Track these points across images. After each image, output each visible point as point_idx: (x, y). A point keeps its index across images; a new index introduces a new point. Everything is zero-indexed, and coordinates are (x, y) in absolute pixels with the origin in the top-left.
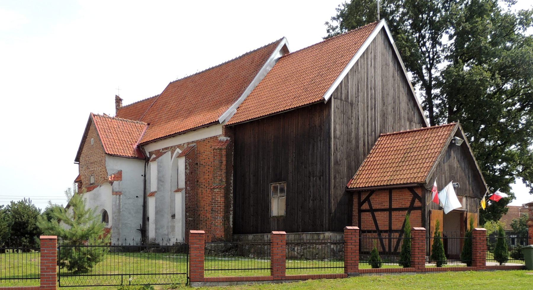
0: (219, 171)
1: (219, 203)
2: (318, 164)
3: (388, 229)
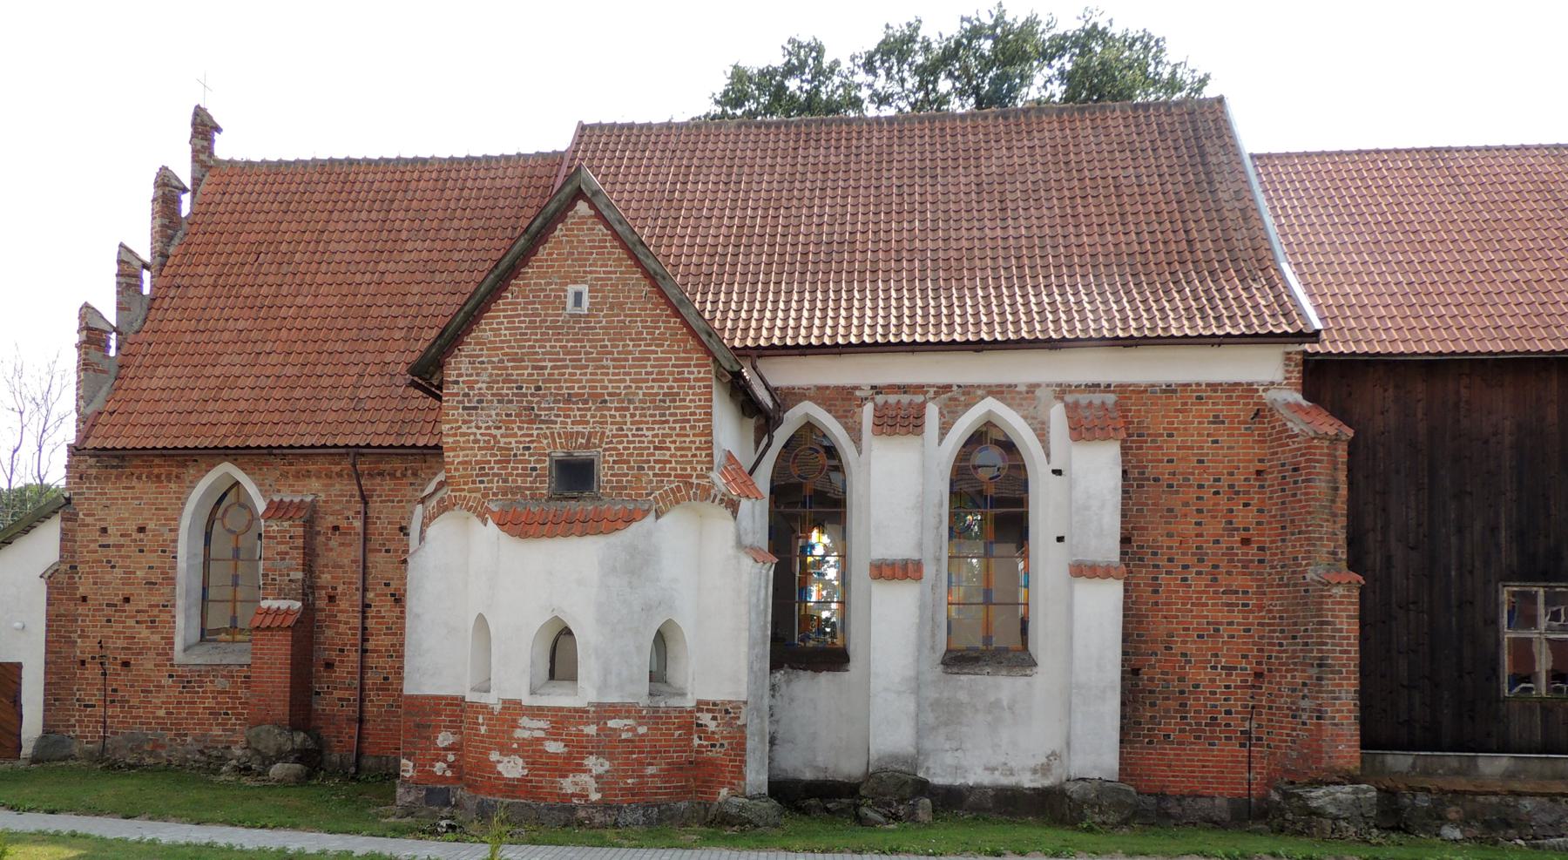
0: (1328, 521)
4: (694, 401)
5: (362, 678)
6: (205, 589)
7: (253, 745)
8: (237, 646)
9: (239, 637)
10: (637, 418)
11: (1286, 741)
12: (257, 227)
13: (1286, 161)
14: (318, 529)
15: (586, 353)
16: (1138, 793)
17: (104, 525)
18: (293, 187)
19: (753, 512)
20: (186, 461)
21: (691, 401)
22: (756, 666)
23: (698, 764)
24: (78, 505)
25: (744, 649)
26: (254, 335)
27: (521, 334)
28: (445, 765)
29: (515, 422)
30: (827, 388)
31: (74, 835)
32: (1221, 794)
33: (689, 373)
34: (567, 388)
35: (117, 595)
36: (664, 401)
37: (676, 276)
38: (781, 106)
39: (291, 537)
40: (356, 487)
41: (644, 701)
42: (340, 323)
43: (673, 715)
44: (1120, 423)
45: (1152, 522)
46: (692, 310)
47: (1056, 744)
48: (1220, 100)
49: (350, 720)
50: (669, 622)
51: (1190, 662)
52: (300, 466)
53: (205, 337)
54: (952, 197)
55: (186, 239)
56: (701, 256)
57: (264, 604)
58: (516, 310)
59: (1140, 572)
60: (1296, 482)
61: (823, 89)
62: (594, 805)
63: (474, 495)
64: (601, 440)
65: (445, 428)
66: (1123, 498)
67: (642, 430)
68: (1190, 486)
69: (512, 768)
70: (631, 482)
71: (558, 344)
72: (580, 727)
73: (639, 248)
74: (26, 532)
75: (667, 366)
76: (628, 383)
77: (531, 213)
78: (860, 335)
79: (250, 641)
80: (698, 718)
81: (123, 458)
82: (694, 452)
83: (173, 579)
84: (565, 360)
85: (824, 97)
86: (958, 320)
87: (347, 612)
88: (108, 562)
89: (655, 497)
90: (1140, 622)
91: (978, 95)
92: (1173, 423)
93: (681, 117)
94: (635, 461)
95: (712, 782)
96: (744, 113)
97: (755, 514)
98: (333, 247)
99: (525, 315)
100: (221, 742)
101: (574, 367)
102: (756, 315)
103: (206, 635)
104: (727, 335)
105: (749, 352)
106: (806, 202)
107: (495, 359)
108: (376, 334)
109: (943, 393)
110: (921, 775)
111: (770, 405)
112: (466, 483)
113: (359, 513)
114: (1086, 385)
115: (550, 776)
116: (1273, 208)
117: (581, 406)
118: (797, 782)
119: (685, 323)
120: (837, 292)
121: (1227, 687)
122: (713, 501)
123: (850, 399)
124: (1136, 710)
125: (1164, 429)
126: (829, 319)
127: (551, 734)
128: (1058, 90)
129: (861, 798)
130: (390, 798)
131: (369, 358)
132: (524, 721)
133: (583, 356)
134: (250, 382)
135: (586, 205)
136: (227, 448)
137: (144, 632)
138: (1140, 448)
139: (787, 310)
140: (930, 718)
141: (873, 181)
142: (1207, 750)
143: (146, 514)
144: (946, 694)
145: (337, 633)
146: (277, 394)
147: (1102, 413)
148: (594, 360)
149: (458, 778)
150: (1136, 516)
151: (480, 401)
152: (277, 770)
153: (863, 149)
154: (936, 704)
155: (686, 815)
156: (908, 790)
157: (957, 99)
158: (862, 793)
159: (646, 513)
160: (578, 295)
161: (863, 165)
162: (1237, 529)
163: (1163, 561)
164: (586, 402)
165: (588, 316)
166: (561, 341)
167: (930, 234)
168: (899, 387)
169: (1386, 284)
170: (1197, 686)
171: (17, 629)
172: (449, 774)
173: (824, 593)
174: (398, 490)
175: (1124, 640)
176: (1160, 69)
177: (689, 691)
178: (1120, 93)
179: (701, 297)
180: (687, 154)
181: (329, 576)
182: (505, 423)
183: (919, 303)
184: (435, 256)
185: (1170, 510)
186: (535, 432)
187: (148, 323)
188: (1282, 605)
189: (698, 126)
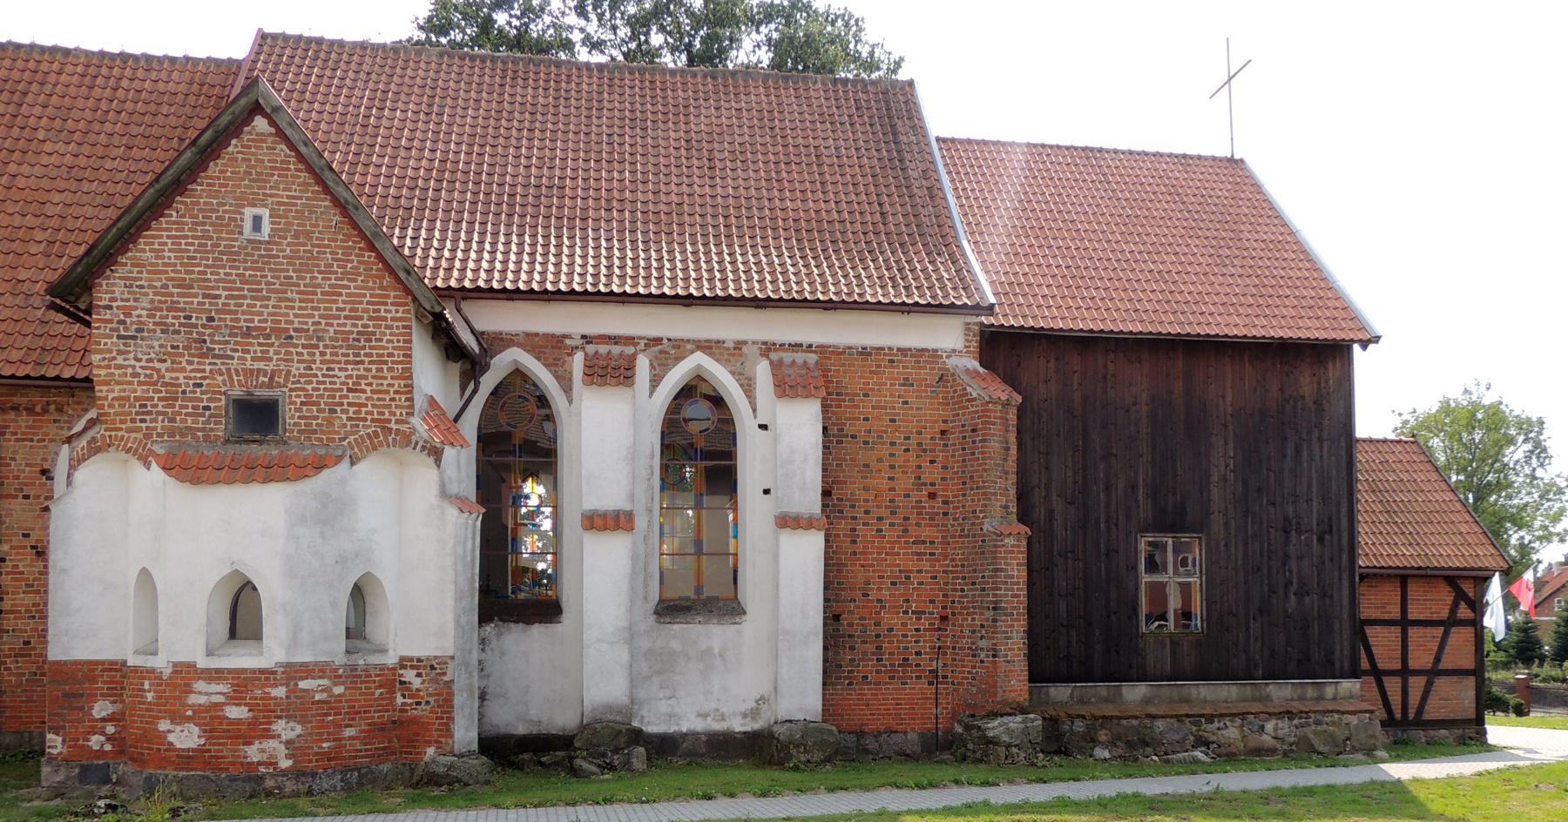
1: (1014, 584)
2: (1314, 499)
3: (1399, 666)
4: (392, 341)
11: (967, 678)
15: (268, 283)
16: (839, 732)
21: (388, 341)
22: (464, 620)
23: (402, 723)
25: (450, 602)
27: (189, 258)
28: (103, 738)
30: (537, 335)
32: (913, 729)
33: (386, 311)
34: (245, 321)
36: (359, 340)
41: (340, 659)
43: (373, 673)
45: (850, 477)
47: (765, 689)
48: (911, 83)
50: (368, 575)
54: (662, 151)
56: (399, 188)
60: (974, 442)
61: (532, 26)
62: (284, 773)
63: (133, 435)
65: (96, 358)
66: (823, 453)
67: (333, 369)
68: (883, 443)
69: (186, 737)
70: (321, 425)
71: (234, 272)
75: (361, 303)
76: (317, 319)
77: (202, 124)
78: (569, 283)
80: (402, 675)
82: (392, 395)
85: (535, 35)
86: (667, 274)
93: (376, 39)
95: (417, 741)
97: (461, 463)
99: (193, 237)
101: (253, 298)
102: (460, 254)
104: (428, 273)
106: (513, 141)
107: (158, 284)
109: (654, 346)
111: (477, 349)
112: (122, 422)
114: (790, 345)
116: (956, 189)
117: (262, 341)
118: (509, 737)
121: (917, 630)
122: (414, 448)
123: (560, 348)
127: (232, 698)
128: (765, 57)
132: (200, 685)
133: (263, 286)
138: (840, 406)
141: (583, 127)
142: (899, 689)
147: (804, 372)
150: (836, 471)
151: (139, 330)
153: (573, 93)
155: (389, 778)
157: (669, 54)
160: (257, 221)
161: (573, 110)
162: (925, 484)
164: (268, 337)
165: (268, 243)
167: (640, 187)
168: (610, 337)
170: (891, 630)
172: (108, 747)
175: (825, 588)
176: (859, 47)
177: (391, 646)
178: (823, 67)
179: (400, 232)
180: (384, 78)
182: (172, 354)
183: (629, 254)
185: (867, 466)
186: (208, 368)
188: (963, 554)
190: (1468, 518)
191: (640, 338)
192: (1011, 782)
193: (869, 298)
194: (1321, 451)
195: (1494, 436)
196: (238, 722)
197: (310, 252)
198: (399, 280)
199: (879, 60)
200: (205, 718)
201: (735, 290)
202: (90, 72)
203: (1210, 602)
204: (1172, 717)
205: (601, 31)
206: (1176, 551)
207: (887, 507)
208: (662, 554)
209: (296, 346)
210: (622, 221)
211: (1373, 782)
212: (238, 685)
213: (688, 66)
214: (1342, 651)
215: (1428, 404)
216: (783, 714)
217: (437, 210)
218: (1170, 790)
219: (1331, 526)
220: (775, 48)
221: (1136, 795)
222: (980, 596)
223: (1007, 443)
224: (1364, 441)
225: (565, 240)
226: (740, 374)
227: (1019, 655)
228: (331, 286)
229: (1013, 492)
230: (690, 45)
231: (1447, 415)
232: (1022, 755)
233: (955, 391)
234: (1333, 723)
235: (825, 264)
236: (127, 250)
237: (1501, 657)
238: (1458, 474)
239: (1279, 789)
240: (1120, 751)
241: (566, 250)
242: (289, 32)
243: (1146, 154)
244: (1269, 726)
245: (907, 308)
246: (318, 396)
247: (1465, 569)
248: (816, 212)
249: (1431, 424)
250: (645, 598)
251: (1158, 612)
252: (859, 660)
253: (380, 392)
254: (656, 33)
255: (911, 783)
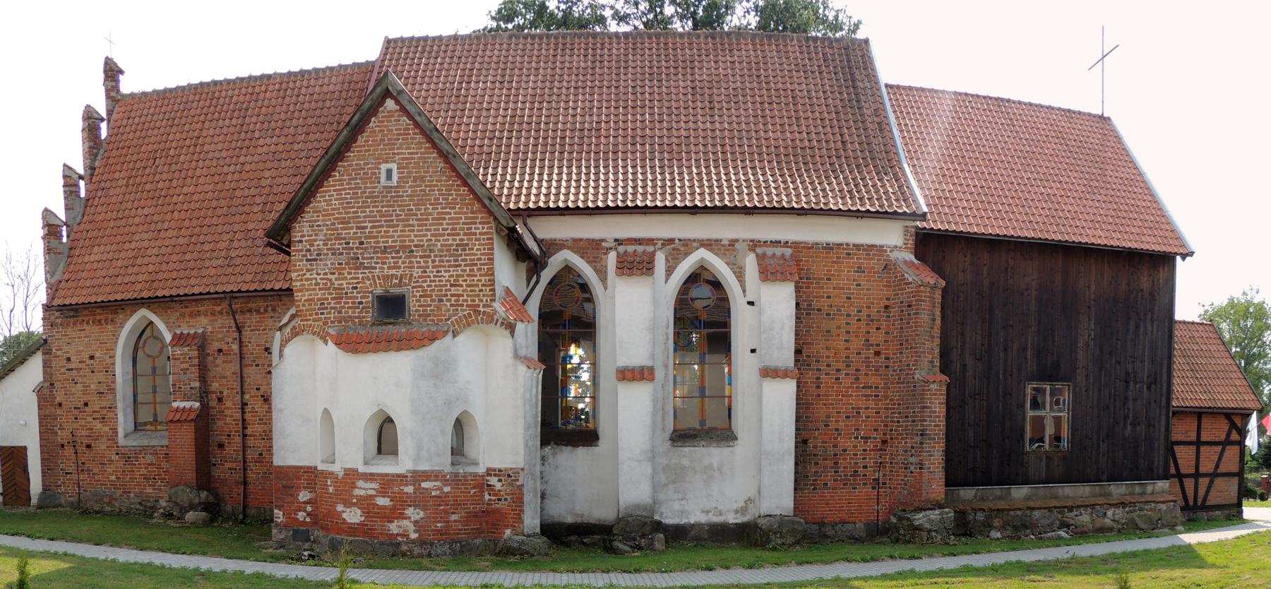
3: (1193, 471)
4: (480, 250)
5: (244, 454)
6: (135, 396)
7: (174, 499)
8: (158, 434)
9: (159, 428)
10: (437, 263)
11: (901, 484)
12: (153, 140)
13: (909, 92)
14: (208, 351)
15: (397, 215)
16: (806, 523)
17: (68, 355)
18: (176, 107)
19: (526, 333)
20: (117, 309)
21: (477, 250)
22: (530, 443)
23: (488, 512)
24: (52, 343)
25: (521, 431)
26: (156, 218)
27: (347, 203)
28: (305, 514)
29: (345, 269)
30: (581, 240)
31: (66, 554)
32: (860, 521)
33: (475, 228)
34: (383, 242)
35: (80, 401)
36: (457, 250)
37: (463, 154)
38: (543, 22)
39: (189, 358)
40: (233, 321)
41: (448, 469)
42: (215, 203)
43: (469, 478)
44: (795, 269)
45: (817, 339)
46: (476, 181)
47: (752, 493)
48: (866, 41)
49: (237, 483)
50: (465, 412)
51: (841, 434)
52: (194, 308)
53: (123, 222)
54: (674, 97)
55: (106, 155)
56: (482, 139)
57: (175, 405)
58: (342, 185)
59: (808, 374)
60: (909, 315)
61: (574, 8)
62: (413, 542)
63: (317, 323)
64: (410, 280)
65: (294, 275)
66: (796, 322)
67: (441, 272)
68: (842, 315)
69: (353, 516)
70: (434, 310)
71: (375, 209)
72: (401, 488)
73: (435, 134)
74: (22, 363)
75: (458, 224)
76: (429, 237)
77: (351, 110)
78: (605, 201)
79: (167, 430)
80: (488, 481)
81: (76, 310)
82: (480, 288)
83: (114, 389)
84: (381, 221)
85: (577, 15)
86: (678, 190)
87: (231, 408)
88: (73, 380)
89: (452, 322)
90: (807, 409)
91: (694, 19)
92: (831, 271)
93: (464, 31)
94: (436, 296)
95: (499, 525)
96: (514, 26)
97: (528, 334)
98: (206, 148)
99: (349, 189)
100: (153, 497)
101: (388, 226)
102: (526, 184)
103: (138, 426)
104: (504, 199)
105: (521, 212)
106: (563, 97)
107: (329, 223)
108: (241, 209)
109: (668, 245)
110: (657, 518)
111: (538, 252)
112: (311, 315)
113: (236, 339)
114: (771, 242)
115: (381, 521)
116: (899, 125)
117: (394, 255)
118: (561, 525)
119: (472, 191)
120: (588, 167)
121: (865, 450)
122: (496, 324)
123: (598, 249)
124: (805, 467)
125: (825, 275)
126: (582, 188)
127: (380, 492)
128: (753, 20)
129: (614, 535)
130: (268, 535)
131: (236, 227)
132: (361, 483)
133: (394, 218)
134: (155, 251)
135: (393, 102)
136: (143, 298)
137: (98, 426)
138: (809, 288)
139: (550, 181)
140: (663, 478)
141: (614, 82)
142: (851, 492)
143: (94, 347)
144: (673, 461)
145: (225, 423)
146: (174, 258)
147: (782, 262)
148: (403, 220)
149: (315, 522)
150: (805, 335)
151: (319, 255)
152: (190, 516)
153: (606, 57)
154: (666, 469)
155: (480, 549)
156: (647, 529)
157: (678, 21)
158: (614, 532)
159: (446, 333)
160: (389, 172)
161: (606, 69)
162: (872, 345)
163: (823, 366)
164: (398, 252)
165: (396, 187)
166: (377, 207)
167: (657, 125)
168: (635, 240)
169: (968, 186)
170: (845, 450)
171: (22, 425)
172: (308, 520)
173: (580, 391)
174: (261, 322)
175: (797, 421)
176: (826, 12)
177: (481, 462)
178: (799, 27)
179: (484, 171)
180: (470, 59)
181: (217, 384)
182: (337, 270)
183: (650, 177)
184: (280, 148)
185: (828, 331)
186: (360, 276)
187: (86, 217)
188: (899, 396)
189: (478, 38)
190: (1241, 376)
191: (658, 239)
192: (931, 556)
193: (832, 206)
194: (1152, 328)
195: (1259, 324)
196: (384, 507)
197: (425, 191)
198: (484, 206)
199: (842, 22)
200: (364, 504)
201: (730, 201)
202: (300, 100)
203: (1074, 429)
204: (1045, 508)
205: (626, 7)
206: (1052, 394)
207: (843, 362)
208: (675, 397)
209: (416, 257)
210: (643, 152)
211: (1174, 546)
212: (384, 484)
213: (694, 29)
214: (1159, 461)
215: (1221, 301)
216: (764, 511)
217: (509, 153)
218: (1042, 558)
219: (1156, 379)
220: (761, 13)
221: (1018, 562)
222: (911, 425)
223: (934, 315)
224: (1180, 322)
225: (602, 169)
226: (733, 264)
227: (938, 468)
228: (438, 214)
229: (937, 351)
230: (695, 13)
231: (1232, 308)
232: (939, 537)
233: (896, 277)
234: (1151, 509)
235: (798, 181)
236: (310, 202)
237: (1254, 464)
238: (1236, 347)
239: (1114, 554)
240: (1009, 533)
241: (602, 177)
242: (405, 36)
243: (1042, 106)
244: (1110, 513)
245: (861, 214)
246: (430, 291)
247: (1236, 409)
248: (792, 140)
249: (1221, 313)
250: (663, 429)
251: (1038, 437)
252: (822, 472)
253: (472, 286)
254: (669, 5)
255: (858, 558)
